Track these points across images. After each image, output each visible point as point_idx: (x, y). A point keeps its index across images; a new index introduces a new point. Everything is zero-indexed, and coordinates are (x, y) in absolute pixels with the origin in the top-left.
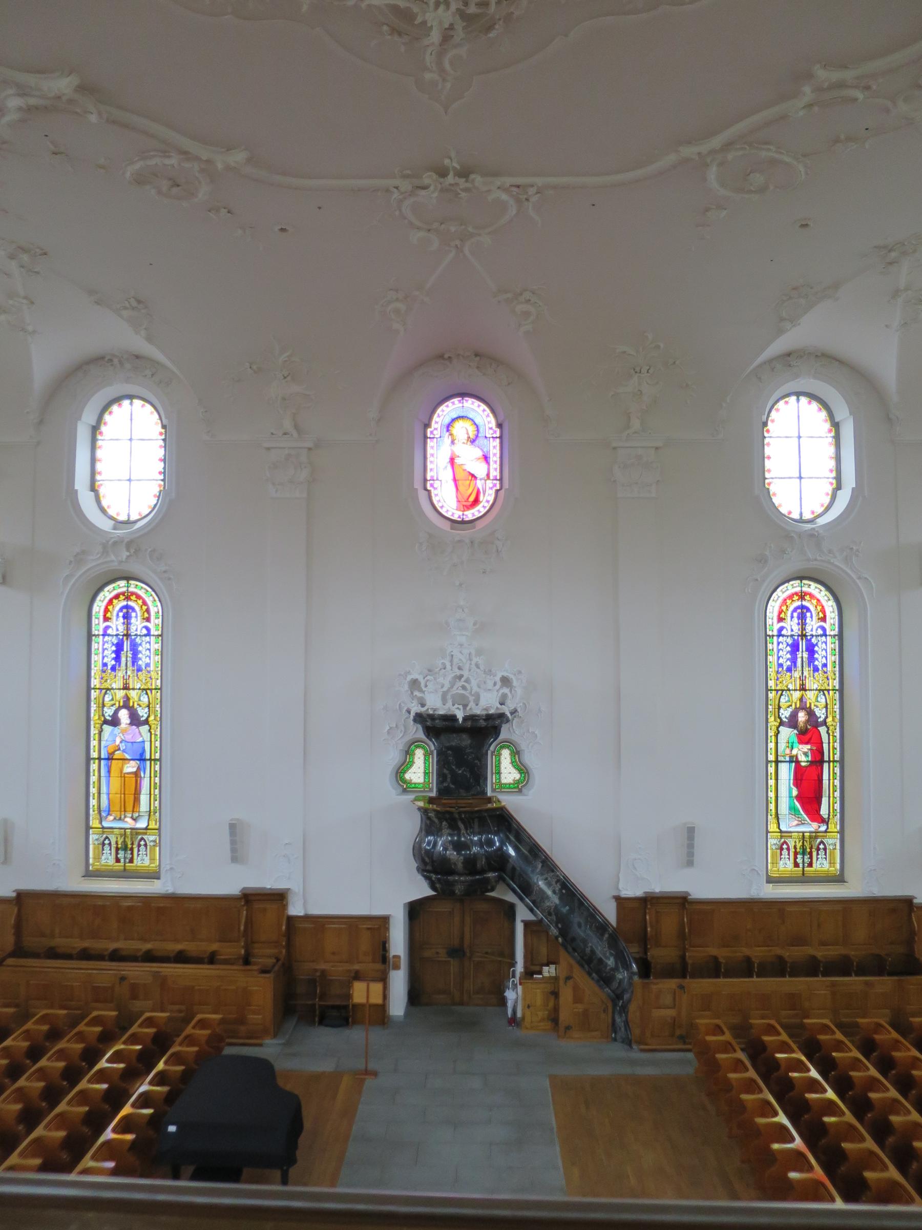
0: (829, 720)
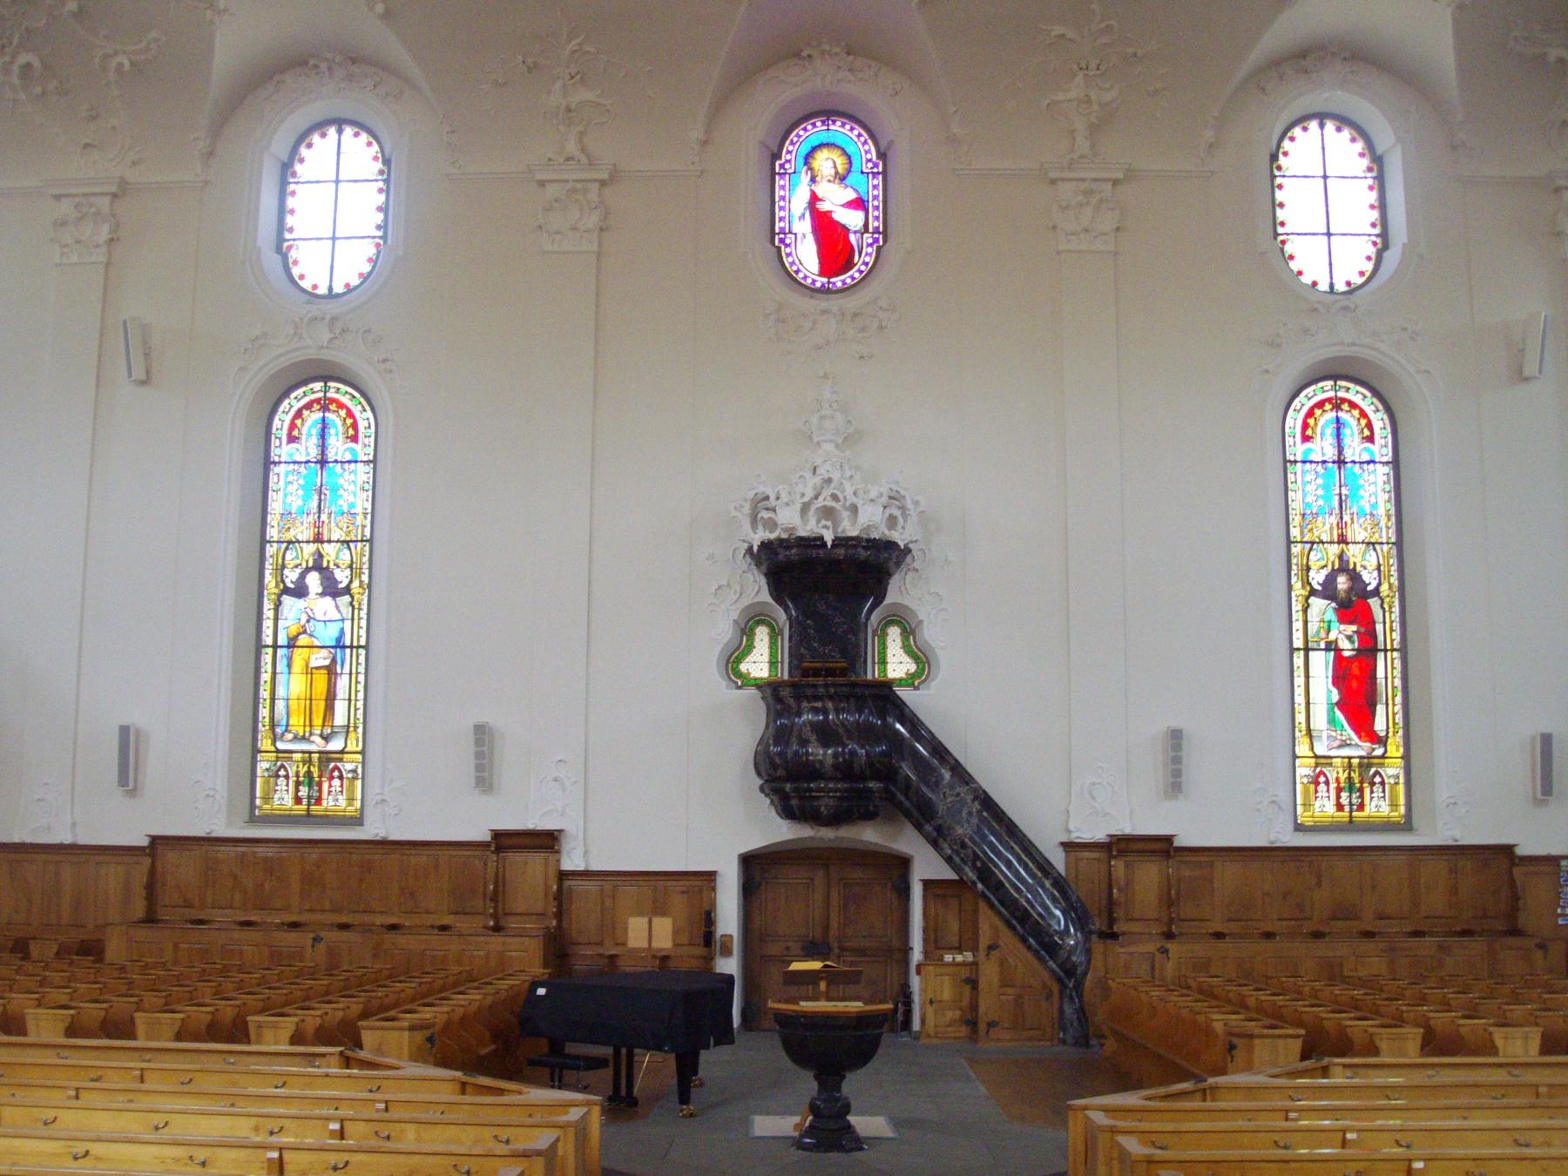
0: (1384, 588)
